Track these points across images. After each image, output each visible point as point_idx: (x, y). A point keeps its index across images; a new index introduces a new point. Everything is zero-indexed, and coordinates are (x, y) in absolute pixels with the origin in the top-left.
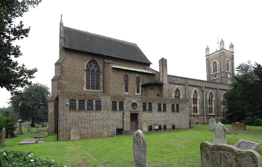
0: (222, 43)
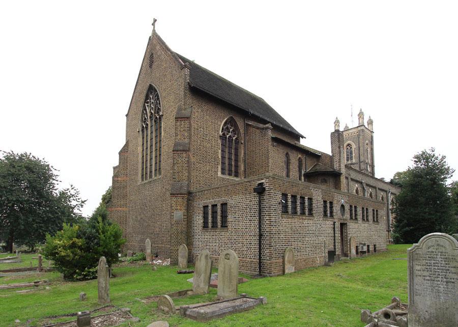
0: (361, 115)
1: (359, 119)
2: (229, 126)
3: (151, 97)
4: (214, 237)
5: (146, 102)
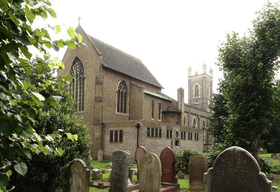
0: (205, 66)
1: (203, 69)
2: (122, 85)
3: (77, 64)
4: (116, 146)
5: (73, 65)
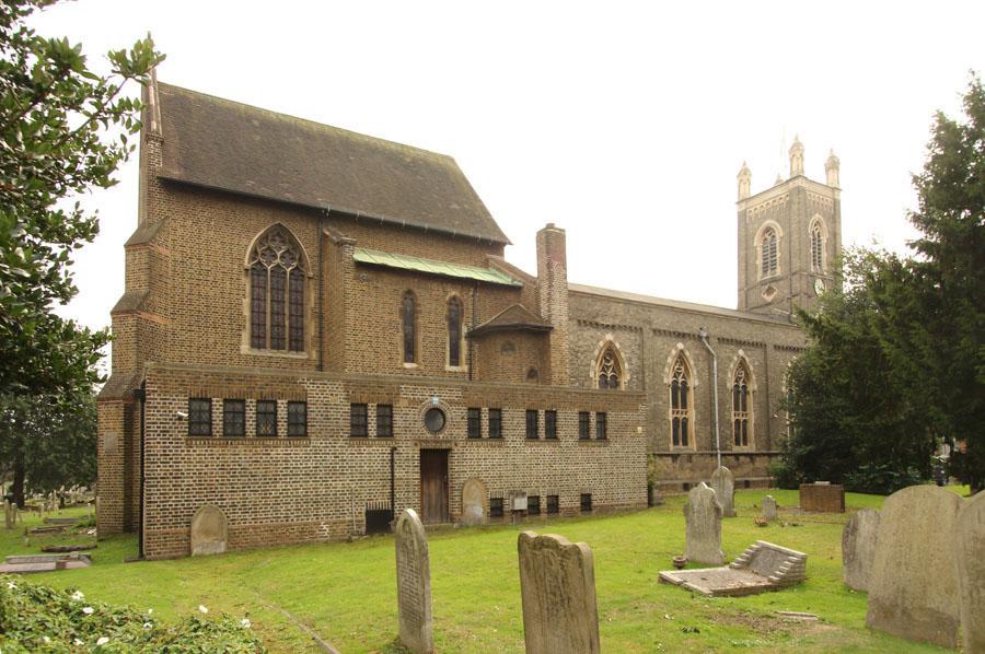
0: (796, 151)
1: (791, 160)
